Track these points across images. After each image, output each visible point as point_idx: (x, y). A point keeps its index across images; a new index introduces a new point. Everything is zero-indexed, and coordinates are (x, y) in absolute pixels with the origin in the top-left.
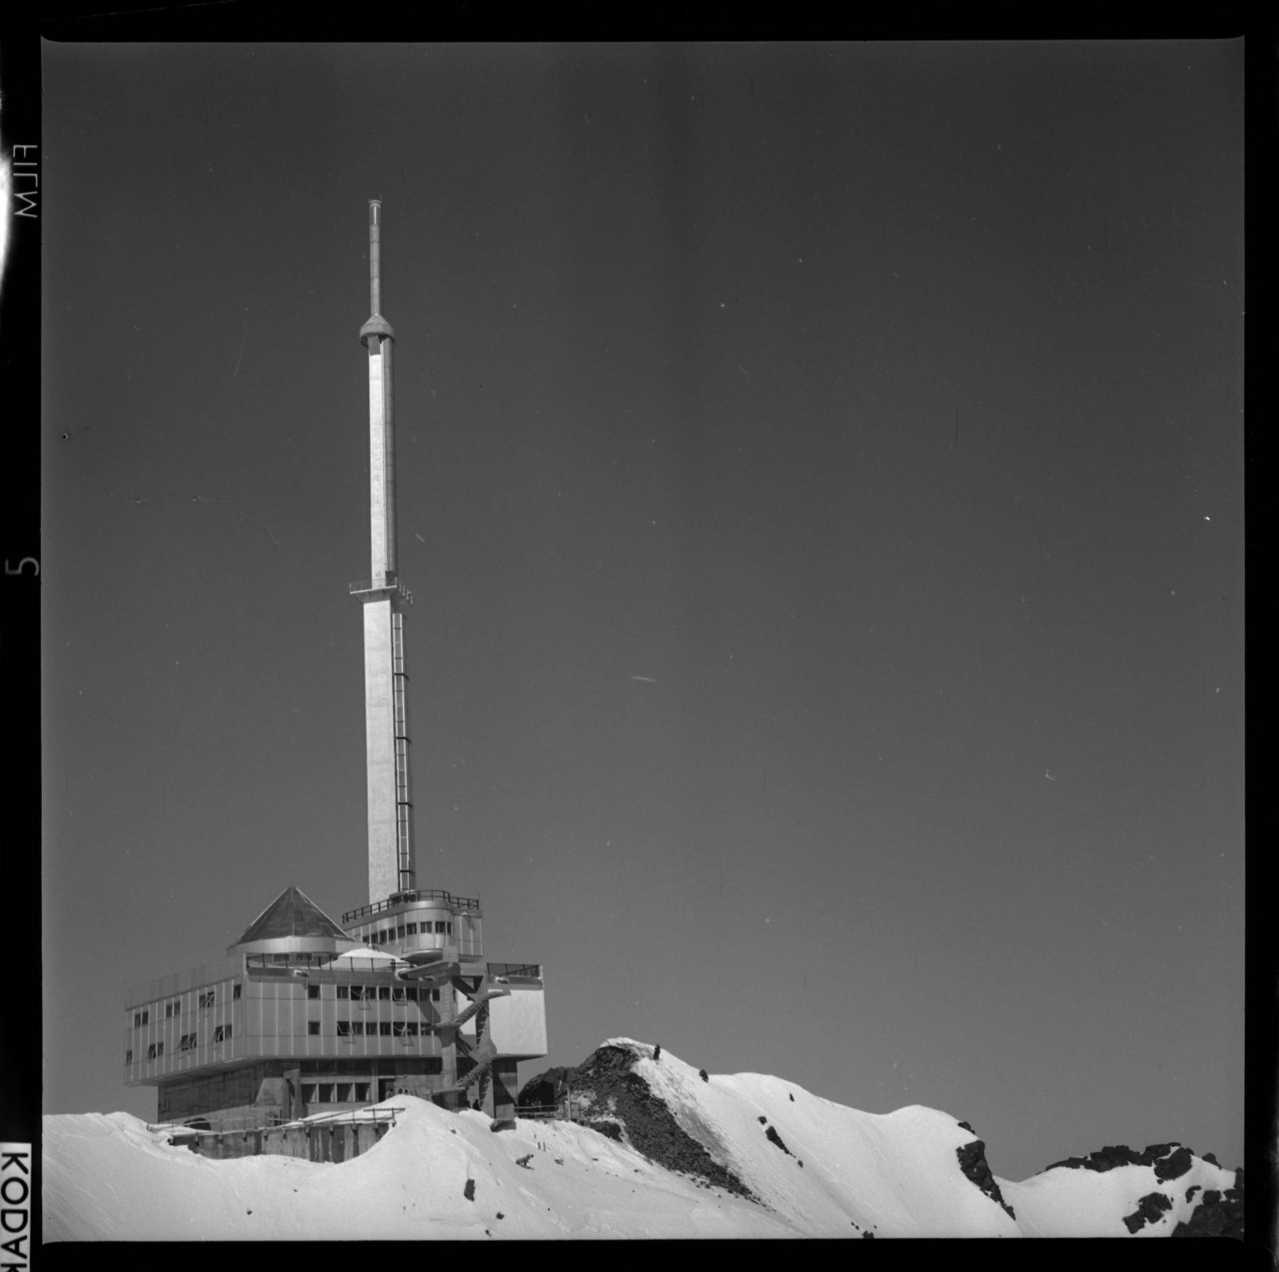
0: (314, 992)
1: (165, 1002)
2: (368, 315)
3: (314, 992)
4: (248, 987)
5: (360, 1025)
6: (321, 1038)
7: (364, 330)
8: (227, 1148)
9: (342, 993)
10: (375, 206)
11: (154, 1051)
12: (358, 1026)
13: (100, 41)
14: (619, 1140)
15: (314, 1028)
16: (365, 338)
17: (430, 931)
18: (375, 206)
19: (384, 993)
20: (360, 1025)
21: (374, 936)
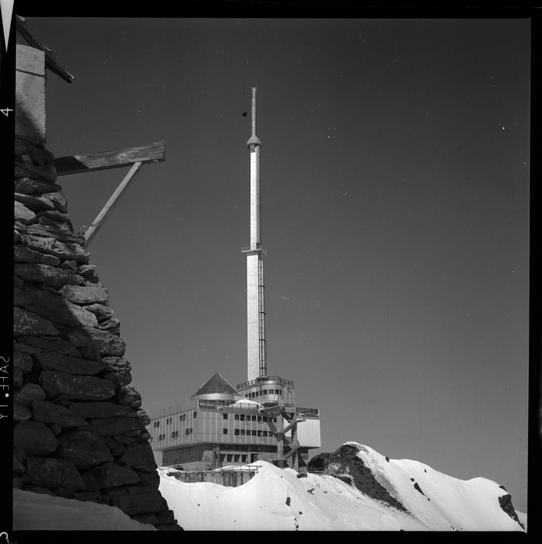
0: (225, 417)
2: (250, 136)
3: (225, 417)
5: (244, 431)
7: (249, 142)
9: (237, 417)
10: (254, 90)
12: (243, 431)
14: (351, 485)
16: (249, 145)
17: (273, 393)
18: (254, 90)
21: (250, 395)
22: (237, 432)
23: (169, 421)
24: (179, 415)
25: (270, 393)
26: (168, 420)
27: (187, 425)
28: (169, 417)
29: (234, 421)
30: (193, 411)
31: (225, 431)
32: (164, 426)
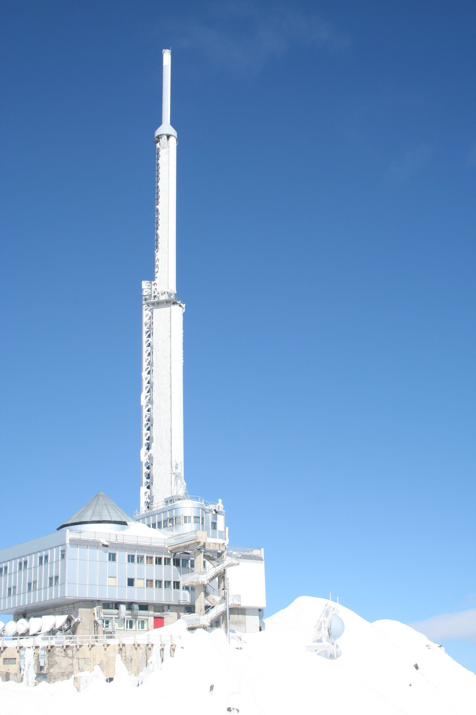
0: (112, 557)
1: (18, 560)
2: (159, 123)
3: (112, 557)
4: (70, 551)
5: (160, 582)
6: (134, 589)
7: (158, 133)
8: (125, 660)
9: (131, 559)
10: (167, 57)
11: (11, 591)
12: (159, 583)
13: (171, 92)
14: (103, 671)
15: (131, 582)
16: (159, 137)
17: (190, 522)
18: (167, 57)
19: (159, 561)
20: (160, 582)
21: (159, 523)
22: (149, 583)
23: (43, 560)
24: (39, 554)
25: (185, 522)
26: (41, 558)
27: (51, 569)
28: (44, 553)
29: (127, 565)
30: (60, 548)
31: (131, 582)
32: (57, 561)
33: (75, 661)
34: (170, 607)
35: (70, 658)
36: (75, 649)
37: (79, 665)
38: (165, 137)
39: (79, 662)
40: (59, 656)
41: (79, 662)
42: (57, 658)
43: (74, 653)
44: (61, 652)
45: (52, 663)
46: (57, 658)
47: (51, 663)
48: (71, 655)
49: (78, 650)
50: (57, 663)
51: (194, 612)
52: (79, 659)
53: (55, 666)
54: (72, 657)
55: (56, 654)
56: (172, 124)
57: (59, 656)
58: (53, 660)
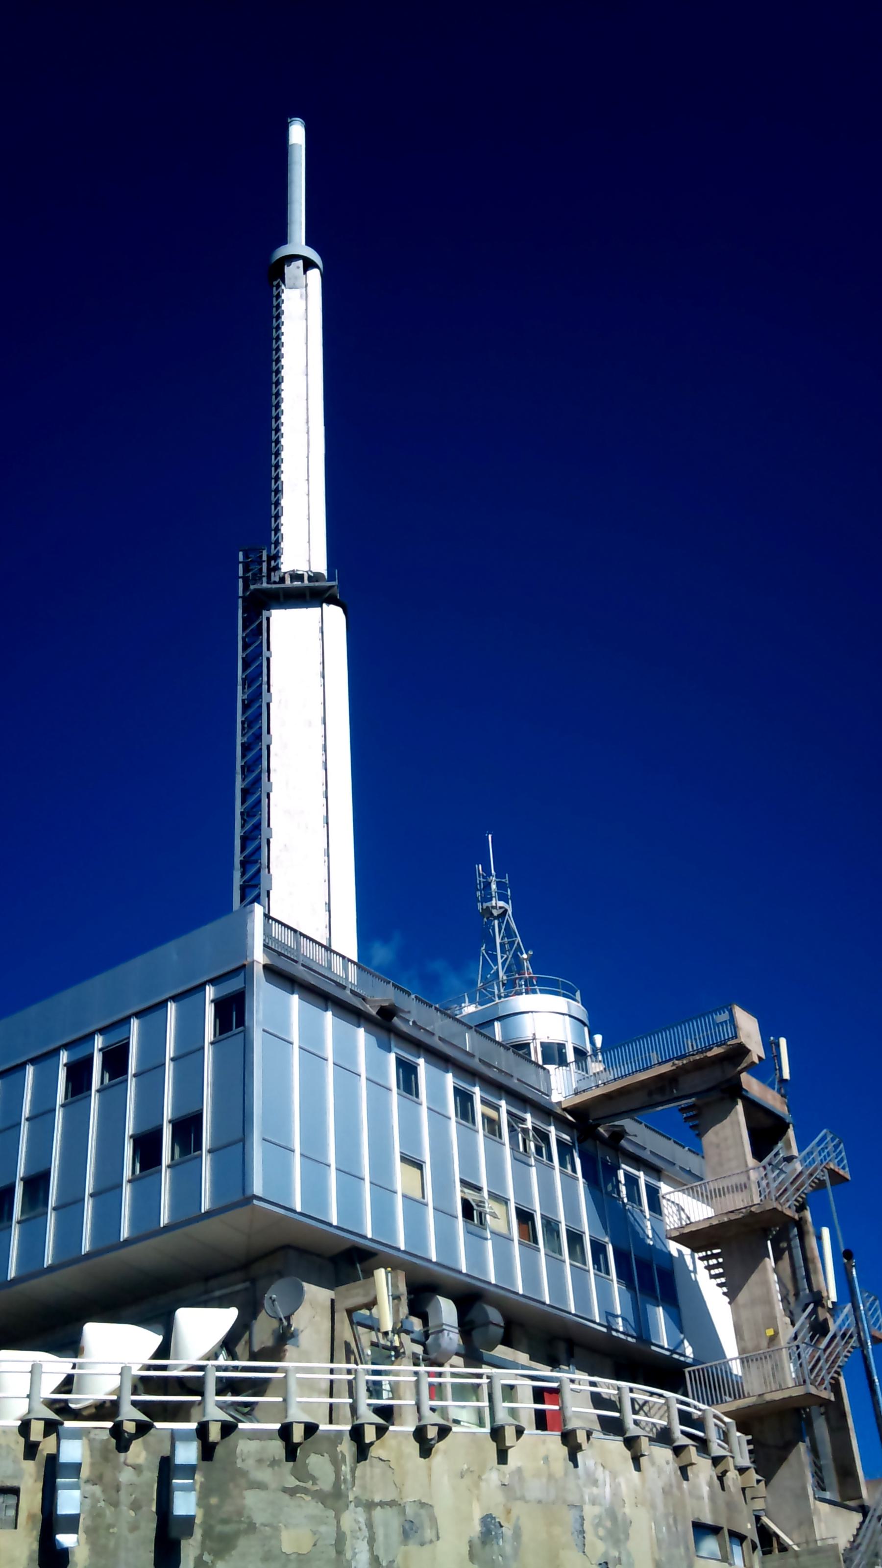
2: (283, 238)
4: (264, 997)
10: (297, 133)
18: (297, 133)
33: (353, 1518)
34: (577, 1351)
35: (321, 1497)
36: (347, 1448)
37: (371, 1541)
38: (300, 263)
39: (370, 1525)
40: (260, 1486)
41: (370, 1525)
42: (252, 1500)
43: (345, 1469)
44: (274, 1463)
45: (227, 1529)
46: (252, 1500)
47: (219, 1528)
48: (326, 1483)
49: (362, 1451)
50: (252, 1527)
51: (499, 1463)
52: (370, 1506)
53: (243, 1543)
54: (334, 1498)
55: (244, 1473)
56: (310, 241)
57: (260, 1486)
58: (228, 1508)
